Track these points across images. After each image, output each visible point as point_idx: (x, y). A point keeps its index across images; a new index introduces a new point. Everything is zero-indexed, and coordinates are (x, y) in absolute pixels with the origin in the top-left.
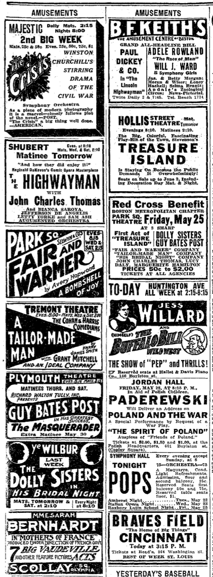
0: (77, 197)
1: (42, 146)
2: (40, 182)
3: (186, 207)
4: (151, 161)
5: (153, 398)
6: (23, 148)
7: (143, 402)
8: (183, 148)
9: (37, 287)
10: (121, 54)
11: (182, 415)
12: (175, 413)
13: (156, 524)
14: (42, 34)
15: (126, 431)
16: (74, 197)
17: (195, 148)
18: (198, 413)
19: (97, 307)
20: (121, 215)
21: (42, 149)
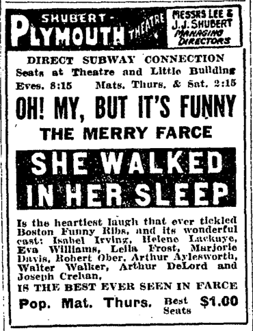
5: (116, 131)
10: (158, 137)
12: (54, 130)
15: (74, 134)
17: (209, 132)
18: (172, 129)
19: (222, 11)
21: (133, 137)
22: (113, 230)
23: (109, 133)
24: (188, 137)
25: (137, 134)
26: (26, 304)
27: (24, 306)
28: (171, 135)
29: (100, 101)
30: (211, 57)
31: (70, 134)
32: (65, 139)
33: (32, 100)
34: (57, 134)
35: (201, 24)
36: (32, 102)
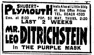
1: (33, 5)
3: (42, 46)
4: (56, 48)
6: (43, 48)
7: (59, 48)
8: (47, 48)
11: (31, 47)
17: (60, 48)
20: (74, 47)
23: (65, 22)
25: (33, 22)
26: (40, 47)
27: (39, 48)
28: (72, 49)
31: (33, 47)
34: (28, 47)
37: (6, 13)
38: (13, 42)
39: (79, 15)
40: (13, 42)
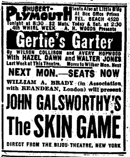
0: (17, 118)
2: (84, 128)
9: (117, 129)
10: (27, 146)
13: (35, 132)
14: (89, 16)
16: (13, 118)
22: (12, 88)
24: (105, 76)
28: (29, 59)
29: (86, 99)
30: (79, 90)
32: (16, 75)
33: (21, 96)
35: (68, 90)
36: (21, 98)
37: (8, 19)
38: (58, 109)
39: (111, 20)
40: (58, 109)
